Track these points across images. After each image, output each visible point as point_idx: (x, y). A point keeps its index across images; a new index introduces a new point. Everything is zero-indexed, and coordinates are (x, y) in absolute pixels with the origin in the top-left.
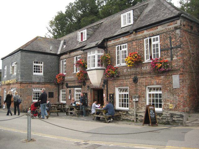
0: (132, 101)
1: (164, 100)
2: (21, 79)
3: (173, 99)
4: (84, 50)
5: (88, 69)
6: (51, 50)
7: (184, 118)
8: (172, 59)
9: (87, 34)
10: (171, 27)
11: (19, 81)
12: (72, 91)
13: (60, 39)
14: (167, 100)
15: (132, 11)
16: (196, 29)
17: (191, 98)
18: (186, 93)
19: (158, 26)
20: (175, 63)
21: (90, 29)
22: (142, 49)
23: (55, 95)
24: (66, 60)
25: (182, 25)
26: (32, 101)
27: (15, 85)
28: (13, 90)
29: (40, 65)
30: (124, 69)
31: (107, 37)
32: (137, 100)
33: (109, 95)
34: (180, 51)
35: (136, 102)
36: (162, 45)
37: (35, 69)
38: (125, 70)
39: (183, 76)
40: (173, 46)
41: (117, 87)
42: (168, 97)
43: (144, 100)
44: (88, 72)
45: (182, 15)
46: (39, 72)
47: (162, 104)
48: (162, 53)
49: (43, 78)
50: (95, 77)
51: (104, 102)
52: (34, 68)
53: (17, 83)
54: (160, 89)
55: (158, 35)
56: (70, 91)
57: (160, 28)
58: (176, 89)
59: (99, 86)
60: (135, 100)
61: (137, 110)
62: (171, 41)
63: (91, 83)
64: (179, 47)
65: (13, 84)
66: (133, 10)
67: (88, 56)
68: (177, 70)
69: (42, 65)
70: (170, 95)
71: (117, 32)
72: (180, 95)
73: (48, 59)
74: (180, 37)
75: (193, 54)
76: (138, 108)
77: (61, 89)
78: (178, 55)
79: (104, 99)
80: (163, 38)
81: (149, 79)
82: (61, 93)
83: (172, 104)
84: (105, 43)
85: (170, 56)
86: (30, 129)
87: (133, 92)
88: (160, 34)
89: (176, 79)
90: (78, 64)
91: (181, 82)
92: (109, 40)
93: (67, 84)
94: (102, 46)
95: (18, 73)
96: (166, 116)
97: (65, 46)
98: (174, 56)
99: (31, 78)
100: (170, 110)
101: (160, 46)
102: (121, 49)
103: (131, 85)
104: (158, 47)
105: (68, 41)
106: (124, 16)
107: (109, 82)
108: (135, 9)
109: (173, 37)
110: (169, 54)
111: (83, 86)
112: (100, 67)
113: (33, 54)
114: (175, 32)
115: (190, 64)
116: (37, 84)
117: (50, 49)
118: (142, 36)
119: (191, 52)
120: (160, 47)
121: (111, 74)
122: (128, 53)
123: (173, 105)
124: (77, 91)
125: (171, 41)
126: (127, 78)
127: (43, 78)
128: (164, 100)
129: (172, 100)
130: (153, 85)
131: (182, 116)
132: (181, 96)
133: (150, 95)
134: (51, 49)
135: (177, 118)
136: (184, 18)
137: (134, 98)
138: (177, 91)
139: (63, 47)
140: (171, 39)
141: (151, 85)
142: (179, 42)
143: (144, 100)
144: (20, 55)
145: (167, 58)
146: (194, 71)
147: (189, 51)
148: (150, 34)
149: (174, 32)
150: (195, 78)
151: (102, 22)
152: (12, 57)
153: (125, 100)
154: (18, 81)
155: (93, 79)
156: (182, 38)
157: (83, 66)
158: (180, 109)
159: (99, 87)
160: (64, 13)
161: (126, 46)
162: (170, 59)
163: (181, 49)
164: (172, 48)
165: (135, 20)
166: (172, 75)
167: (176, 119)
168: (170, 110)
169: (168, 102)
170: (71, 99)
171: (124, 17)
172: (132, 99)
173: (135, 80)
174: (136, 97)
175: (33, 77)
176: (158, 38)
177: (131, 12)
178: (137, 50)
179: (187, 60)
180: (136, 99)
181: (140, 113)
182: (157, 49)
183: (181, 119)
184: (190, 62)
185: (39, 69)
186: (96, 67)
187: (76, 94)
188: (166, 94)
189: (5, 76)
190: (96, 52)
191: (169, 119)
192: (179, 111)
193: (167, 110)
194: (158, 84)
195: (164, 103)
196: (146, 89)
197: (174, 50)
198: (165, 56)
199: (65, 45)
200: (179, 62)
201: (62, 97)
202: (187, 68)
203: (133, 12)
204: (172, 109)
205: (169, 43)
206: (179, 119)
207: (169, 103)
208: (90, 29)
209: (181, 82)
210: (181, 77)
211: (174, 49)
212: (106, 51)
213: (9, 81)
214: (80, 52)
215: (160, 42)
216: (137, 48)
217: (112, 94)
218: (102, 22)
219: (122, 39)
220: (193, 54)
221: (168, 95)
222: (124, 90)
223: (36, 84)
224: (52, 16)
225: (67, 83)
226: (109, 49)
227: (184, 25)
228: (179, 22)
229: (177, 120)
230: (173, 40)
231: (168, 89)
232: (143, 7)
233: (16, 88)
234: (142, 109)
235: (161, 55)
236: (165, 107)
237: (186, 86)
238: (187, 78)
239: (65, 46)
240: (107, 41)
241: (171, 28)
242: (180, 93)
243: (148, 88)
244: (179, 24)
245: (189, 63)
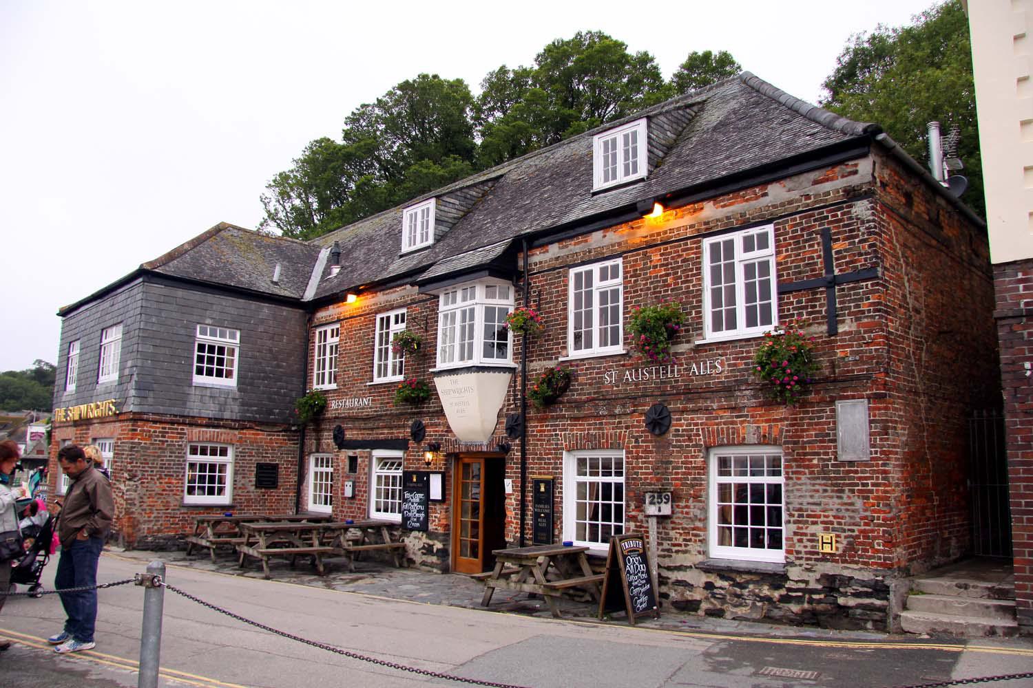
0: (640, 517)
1: (796, 514)
2: (137, 401)
4: (422, 284)
5: (440, 366)
6: (276, 283)
7: (891, 596)
8: (833, 331)
9: (438, 221)
10: (827, 186)
11: (131, 407)
12: (359, 460)
13: (316, 243)
14: (808, 516)
15: (643, 122)
16: (923, 208)
17: (913, 507)
18: (897, 485)
20: (848, 346)
21: (452, 201)
22: (691, 281)
23: (287, 477)
24: (338, 326)
26: (182, 498)
27: (110, 427)
30: (607, 369)
31: (527, 229)
32: (666, 509)
33: (529, 486)
35: (662, 519)
36: (789, 268)
37: (201, 359)
38: (611, 376)
39: (886, 408)
40: (836, 272)
41: (569, 451)
42: (815, 500)
43: (698, 512)
44: (441, 384)
45: (881, 137)
46: (220, 373)
47: (786, 530)
48: (787, 304)
50: (472, 406)
51: (508, 513)
52: (196, 353)
53: (118, 417)
56: (353, 460)
57: (777, 193)
58: (851, 463)
59: (485, 443)
60: (657, 513)
61: (664, 556)
62: (828, 250)
63: (449, 430)
64: (869, 274)
65: (103, 420)
66: (649, 118)
67: (442, 307)
68: (858, 378)
70: (825, 491)
72: (871, 491)
73: (262, 321)
74: (870, 233)
75: (917, 311)
76: (666, 546)
77: (310, 453)
78: (863, 312)
79: (507, 501)
80: (791, 238)
81: (722, 417)
82: (312, 468)
83: (833, 535)
84: (521, 255)
85: (823, 317)
86: (151, 664)
87: (645, 471)
88: (625, 252)
89: (853, 420)
90: (404, 344)
91: (879, 434)
92: (537, 243)
94: (506, 268)
95: (127, 372)
96: (802, 586)
97: (336, 270)
98: (844, 315)
99: (183, 400)
100: (825, 558)
101: (778, 270)
103: (637, 441)
104: (233, 355)
105: (350, 252)
106: (606, 143)
107: (534, 427)
108: (656, 115)
109: (838, 233)
110: (821, 306)
111: (412, 444)
113: (196, 296)
114: (849, 212)
115: (908, 357)
116: (207, 426)
117: (274, 277)
118: (692, 226)
119: (910, 300)
120: (779, 276)
121: (544, 396)
122: (625, 298)
123: (838, 536)
124: (384, 462)
125: (828, 250)
126: (617, 411)
127: (234, 399)
128: (796, 514)
129: (833, 513)
130: (742, 443)
131: (880, 590)
132: (877, 498)
133: (724, 490)
134: (275, 279)
136: (886, 152)
137: (652, 503)
138: (856, 472)
139: (330, 274)
140: (828, 238)
141: (734, 445)
142: (867, 254)
143: (698, 512)
144: (139, 296)
145: (810, 325)
146: (920, 387)
147: (904, 296)
148: (728, 218)
149: (843, 208)
150: (927, 419)
151: (502, 176)
152: (106, 304)
153: (607, 508)
154: (125, 410)
155: (463, 411)
156: (880, 236)
157: (417, 350)
158: (870, 557)
159: (485, 449)
160: (339, 140)
161: (615, 268)
162: (824, 328)
163: (878, 284)
164: (832, 283)
166: (832, 401)
167: (852, 602)
168: (825, 558)
169: (814, 523)
170: (353, 497)
171: (606, 150)
172: (640, 508)
173: (658, 423)
175: (194, 396)
176: (617, 266)
177: (641, 127)
178: (669, 285)
179: (900, 336)
180: (663, 505)
181: (679, 568)
182: (765, 285)
183: (878, 602)
184: (909, 345)
185: (220, 362)
186: (478, 359)
187: (379, 477)
188: (804, 487)
189: (71, 387)
190: (480, 292)
191: (819, 602)
193: (807, 559)
194: (764, 441)
195: (793, 527)
196: (706, 462)
198: (800, 315)
199: (337, 263)
200: (868, 344)
201: (315, 485)
202: (898, 373)
203: (649, 126)
204: (832, 555)
205: (819, 257)
206: (867, 601)
207: (818, 529)
208: (452, 201)
209: (879, 434)
210: (879, 409)
211: (845, 286)
212: (523, 293)
213: (83, 407)
214: (408, 291)
215: (778, 253)
216: (670, 280)
217: (547, 482)
218: (499, 173)
219: (597, 239)
220: (917, 311)
221: (817, 491)
224: (288, 154)
225: (340, 427)
226: (537, 282)
227: (884, 185)
228: (865, 168)
229: (859, 606)
230: (837, 246)
231: (815, 462)
232: (688, 111)
233: (112, 441)
234: (685, 552)
235: (779, 311)
236: (798, 547)
237: (896, 453)
238: (900, 416)
239: (336, 270)
240: (531, 248)
241: (828, 193)
242: (873, 485)
244: (869, 178)
245: (903, 349)
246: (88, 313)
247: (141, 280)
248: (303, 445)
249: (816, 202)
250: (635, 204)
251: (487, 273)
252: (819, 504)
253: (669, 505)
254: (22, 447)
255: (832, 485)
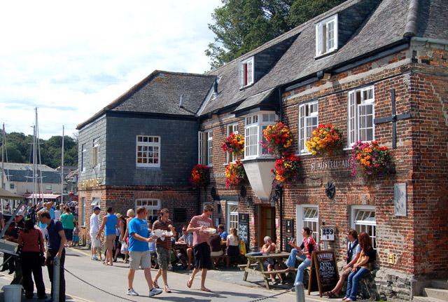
3: (395, 241)
19: (371, 62)
25: (420, 61)
28: (96, 203)
29: (153, 144)
31: (285, 81)
34: (410, 125)
37: (140, 154)
49: (159, 175)
52: (137, 151)
54: (373, 215)
55: (372, 84)
57: (376, 70)
69: (158, 144)
71: (235, 97)
77: (203, 202)
93: (214, 190)
102: (307, 115)
112: (268, 156)
116: (146, 190)
121: (292, 174)
135: (400, 286)
148: (357, 81)
151: (299, 34)
158: (407, 267)
162: (391, 144)
165: (343, 40)
167: (397, 290)
169: (387, 248)
174: (328, 230)
180: (330, 235)
188: (383, 229)
192: (405, 270)
193: (384, 266)
197: (398, 123)
222: (363, 212)
223: (142, 190)
230: (398, 99)
241: (394, 69)
243: (357, 210)
246: (87, 130)
247: (105, 115)
248: (199, 198)
249: (390, 74)
250: (316, 73)
251: (259, 108)
252: (388, 238)
253: (333, 235)
254: (357, 18)
255: (393, 228)
